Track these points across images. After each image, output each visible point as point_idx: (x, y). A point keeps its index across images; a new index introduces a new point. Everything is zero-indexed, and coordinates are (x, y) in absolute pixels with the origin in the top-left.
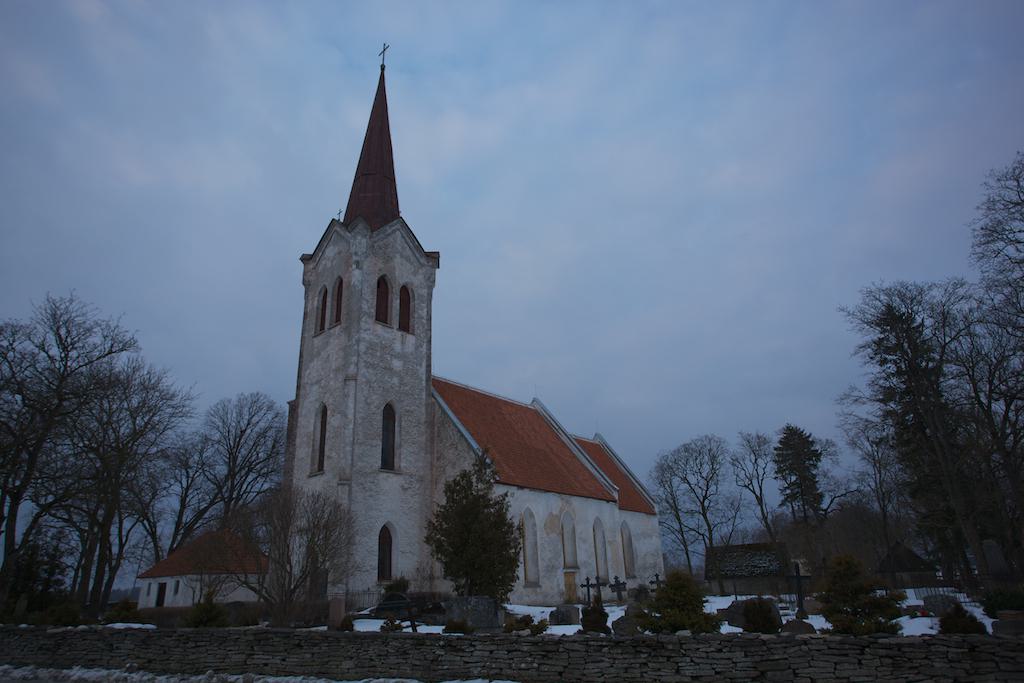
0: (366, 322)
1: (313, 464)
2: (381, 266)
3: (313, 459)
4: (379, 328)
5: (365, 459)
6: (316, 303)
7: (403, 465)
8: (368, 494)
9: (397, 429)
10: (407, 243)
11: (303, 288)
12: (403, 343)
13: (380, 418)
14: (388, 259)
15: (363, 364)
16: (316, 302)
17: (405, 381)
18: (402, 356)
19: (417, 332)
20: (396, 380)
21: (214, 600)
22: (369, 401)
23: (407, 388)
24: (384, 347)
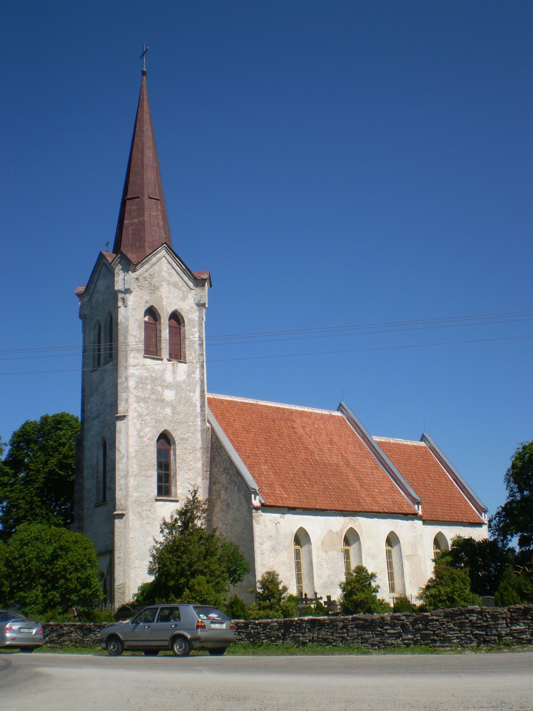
0: (134, 358)
2: (147, 297)
6: (92, 337)
8: (145, 521)
11: (80, 322)
12: (174, 372)
14: (154, 289)
15: (134, 400)
16: (93, 335)
18: (176, 386)
19: (189, 358)
21: (418, 603)
22: (142, 434)
23: (180, 417)
24: (154, 380)
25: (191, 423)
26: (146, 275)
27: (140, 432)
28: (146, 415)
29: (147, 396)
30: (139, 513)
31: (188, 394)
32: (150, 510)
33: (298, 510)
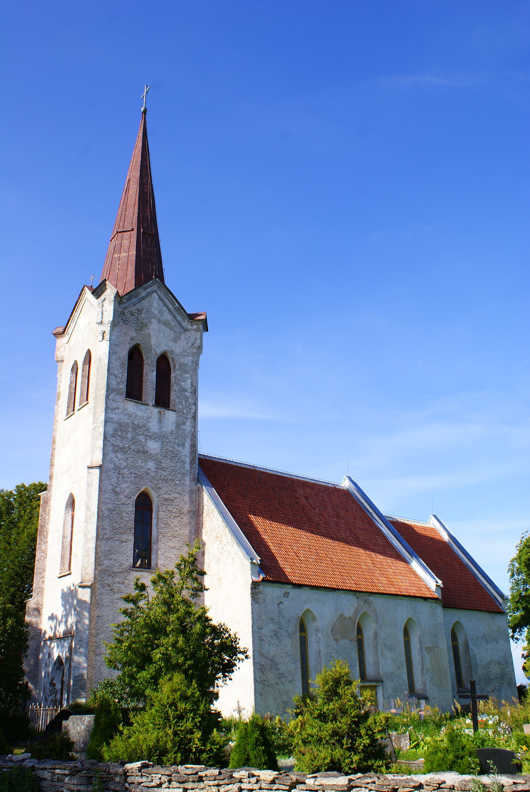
1: (62, 563)
3: (62, 557)
4: (131, 406)
5: (114, 557)
7: (160, 562)
9: (154, 521)
10: (165, 305)
13: (131, 509)
14: (142, 326)
17: (164, 465)
20: (151, 465)
22: (117, 490)
23: (165, 473)
24: (136, 427)
25: (178, 482)
26: (133, 309)
27: (116, 487)
28: (124, 468)
29: (126, 446)
30: (109, 585)
31: (176, 447)
32: (123, 583)
33: (429, 600)
